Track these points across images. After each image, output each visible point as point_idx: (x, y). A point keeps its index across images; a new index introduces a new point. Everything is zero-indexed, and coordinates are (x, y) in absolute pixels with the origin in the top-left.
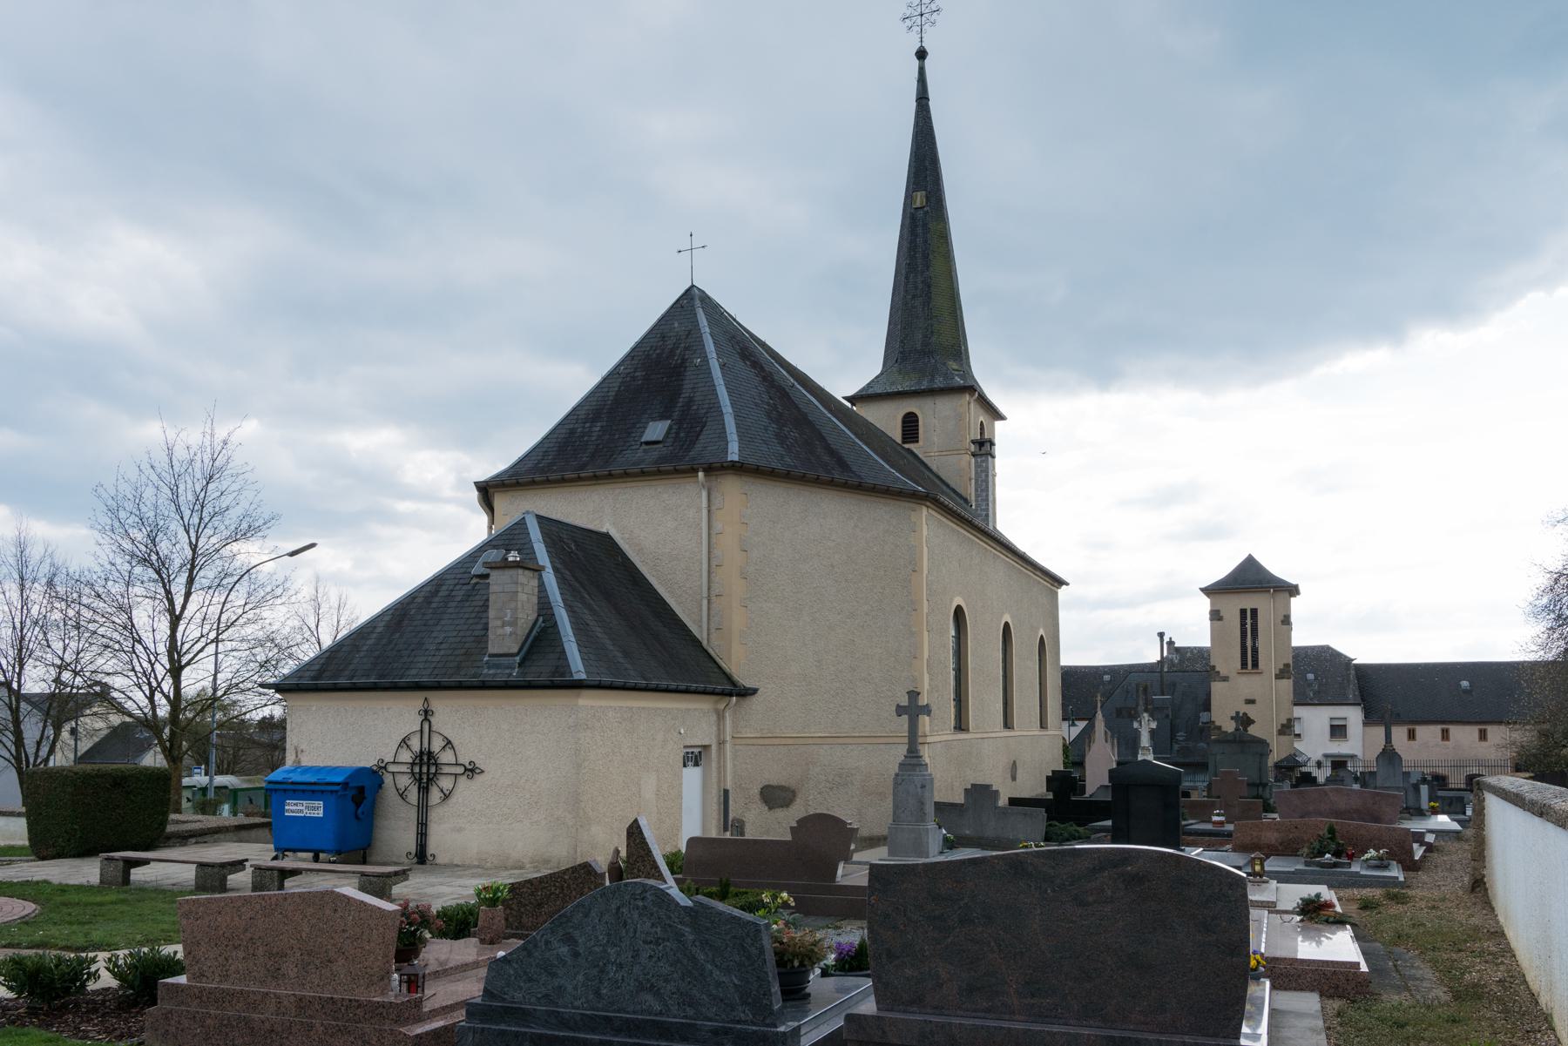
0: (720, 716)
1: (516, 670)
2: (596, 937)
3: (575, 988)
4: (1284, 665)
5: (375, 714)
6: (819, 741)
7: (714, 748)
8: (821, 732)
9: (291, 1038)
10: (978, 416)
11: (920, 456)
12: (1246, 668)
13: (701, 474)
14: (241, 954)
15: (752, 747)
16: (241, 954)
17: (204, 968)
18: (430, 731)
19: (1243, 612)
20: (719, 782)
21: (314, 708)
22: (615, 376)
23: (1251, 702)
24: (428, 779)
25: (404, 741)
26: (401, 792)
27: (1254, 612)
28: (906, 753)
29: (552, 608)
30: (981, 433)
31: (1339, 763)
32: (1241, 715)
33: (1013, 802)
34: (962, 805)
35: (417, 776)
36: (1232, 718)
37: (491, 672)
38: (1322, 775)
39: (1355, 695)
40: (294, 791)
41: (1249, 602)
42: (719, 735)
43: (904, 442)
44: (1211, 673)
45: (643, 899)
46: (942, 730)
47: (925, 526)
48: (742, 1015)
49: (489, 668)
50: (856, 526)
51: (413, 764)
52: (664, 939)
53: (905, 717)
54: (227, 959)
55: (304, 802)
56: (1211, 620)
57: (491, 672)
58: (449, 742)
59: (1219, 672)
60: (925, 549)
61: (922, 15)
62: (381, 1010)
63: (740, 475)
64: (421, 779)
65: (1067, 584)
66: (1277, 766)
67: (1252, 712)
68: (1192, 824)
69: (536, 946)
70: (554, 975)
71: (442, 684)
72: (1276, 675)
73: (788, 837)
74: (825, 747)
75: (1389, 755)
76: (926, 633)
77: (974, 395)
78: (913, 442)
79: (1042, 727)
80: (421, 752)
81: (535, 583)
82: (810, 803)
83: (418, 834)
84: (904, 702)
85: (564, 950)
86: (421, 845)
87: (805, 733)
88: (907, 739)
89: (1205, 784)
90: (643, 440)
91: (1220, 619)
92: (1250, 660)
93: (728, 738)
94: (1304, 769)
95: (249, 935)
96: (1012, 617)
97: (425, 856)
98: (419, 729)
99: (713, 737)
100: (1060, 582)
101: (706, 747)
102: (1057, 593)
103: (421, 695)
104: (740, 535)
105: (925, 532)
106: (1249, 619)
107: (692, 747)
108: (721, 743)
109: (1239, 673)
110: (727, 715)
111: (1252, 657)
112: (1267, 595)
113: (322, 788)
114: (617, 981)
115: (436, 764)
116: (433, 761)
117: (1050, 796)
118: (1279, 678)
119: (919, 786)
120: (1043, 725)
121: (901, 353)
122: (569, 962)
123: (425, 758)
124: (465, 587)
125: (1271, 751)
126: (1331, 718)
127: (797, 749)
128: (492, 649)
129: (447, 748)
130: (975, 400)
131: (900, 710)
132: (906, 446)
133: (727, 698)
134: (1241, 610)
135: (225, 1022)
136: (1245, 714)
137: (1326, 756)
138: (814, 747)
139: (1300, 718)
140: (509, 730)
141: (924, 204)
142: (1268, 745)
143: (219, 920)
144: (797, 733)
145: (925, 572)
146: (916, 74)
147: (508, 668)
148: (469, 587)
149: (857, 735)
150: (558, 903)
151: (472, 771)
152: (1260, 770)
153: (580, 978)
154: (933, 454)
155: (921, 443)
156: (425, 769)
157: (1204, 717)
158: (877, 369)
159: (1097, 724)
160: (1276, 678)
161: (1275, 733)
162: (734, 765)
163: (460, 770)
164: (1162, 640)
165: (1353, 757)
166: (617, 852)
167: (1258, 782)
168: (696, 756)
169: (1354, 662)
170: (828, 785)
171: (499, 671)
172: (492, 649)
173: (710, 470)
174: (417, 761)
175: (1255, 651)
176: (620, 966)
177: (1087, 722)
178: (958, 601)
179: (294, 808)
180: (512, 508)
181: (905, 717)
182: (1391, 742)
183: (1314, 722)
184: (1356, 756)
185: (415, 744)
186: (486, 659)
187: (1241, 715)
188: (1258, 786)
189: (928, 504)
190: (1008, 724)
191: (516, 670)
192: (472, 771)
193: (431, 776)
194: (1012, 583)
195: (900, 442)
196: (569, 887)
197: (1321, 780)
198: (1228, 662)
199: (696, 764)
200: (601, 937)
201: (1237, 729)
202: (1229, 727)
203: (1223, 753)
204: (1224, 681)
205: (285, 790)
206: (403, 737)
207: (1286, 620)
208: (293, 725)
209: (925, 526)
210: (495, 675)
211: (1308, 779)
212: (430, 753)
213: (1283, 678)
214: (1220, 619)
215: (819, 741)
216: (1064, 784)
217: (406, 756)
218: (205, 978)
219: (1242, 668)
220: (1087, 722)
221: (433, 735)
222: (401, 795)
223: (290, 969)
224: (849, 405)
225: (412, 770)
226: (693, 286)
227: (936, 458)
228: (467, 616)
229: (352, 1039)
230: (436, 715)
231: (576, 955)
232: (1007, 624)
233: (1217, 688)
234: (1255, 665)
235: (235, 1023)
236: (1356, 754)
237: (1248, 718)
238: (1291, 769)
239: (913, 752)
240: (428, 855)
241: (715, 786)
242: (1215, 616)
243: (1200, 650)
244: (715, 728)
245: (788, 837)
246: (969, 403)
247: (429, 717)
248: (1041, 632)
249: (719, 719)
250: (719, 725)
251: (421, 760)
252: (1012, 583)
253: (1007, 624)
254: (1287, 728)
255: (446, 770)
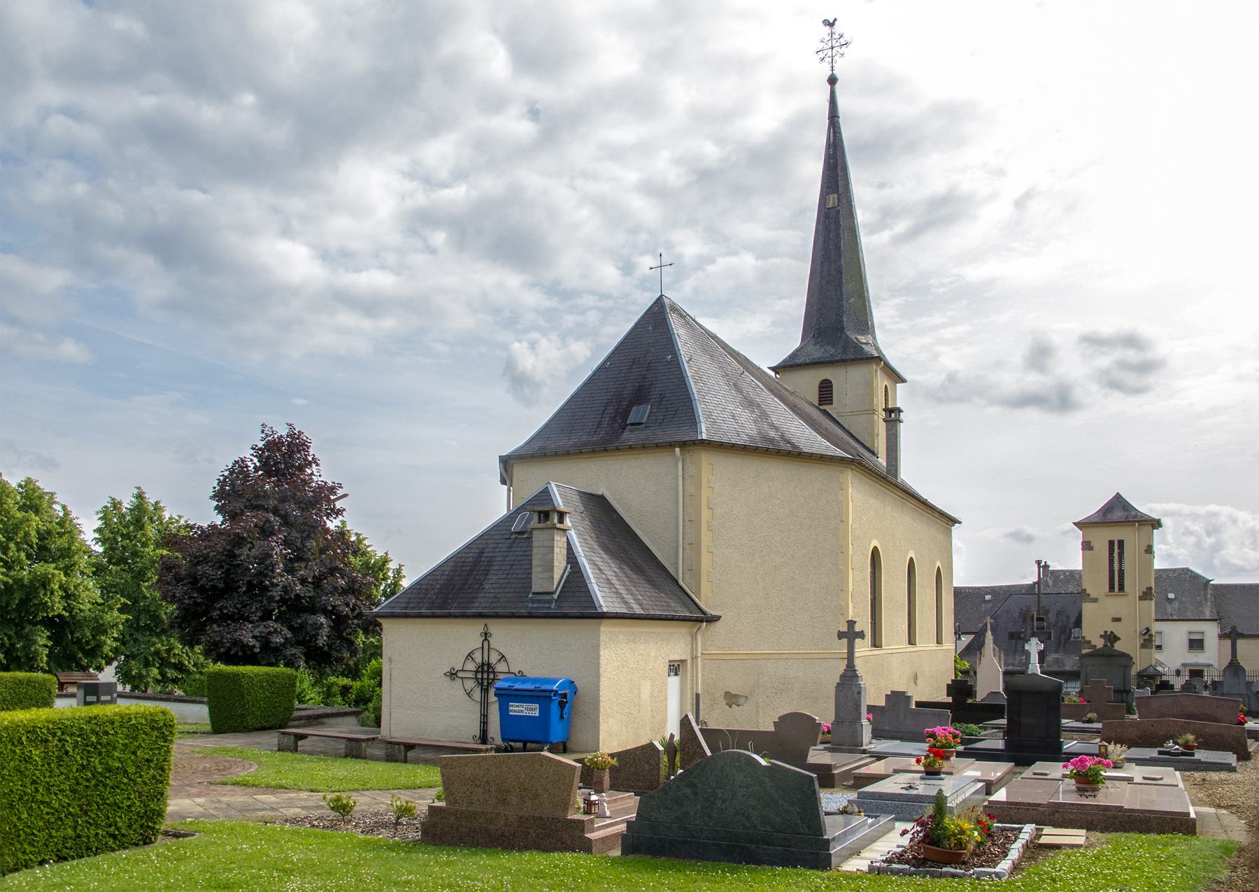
0: (694, 638)
1: (554, 604)
2: (709, 783)
3: (696, 814)
4: (1147, 588)
5: (447, 634)
6: (767, 657)
7: (689, 662)
8: (769, 650)
9: (515, 840)
10: (881, 381)
11: (834, 416)
12: (1114, 591)
13: (677, 450)
14: (480, 790)
15: (715, 661)
16: (480, 790)
17: (458, 798)
18: (489, 648)
19: (1111, 543)
20: (692, 688)
21: (403, 630)
22: (603, 370)
23: (1118, 620)
24: (488, 683)
25: (469, 655)
26: (468, 692)
27: (1121, 543)
28: (845, 668)
29: (576, 558)
30: (885, 404)
31: (1196, 673)
32: (1109, 633)
33: (919, 704)
34: (883, 707)
35: (480, 681)
36: (1101, 636)
37: (535, 605)
38: (1178, 683)
39: (1211, 611)
40: (517, 696)
41: (1116, 534)
42: (693, 651)
43: (820, 405)
44: (1083, 595)
45: (738, 762)
46: (862, 648)
47: (850, 485)
48: (802, 829)
49: (533, 603)
50: (797, 487)
51: (477, 672)
52: (752, 785)
53: (845, 641)
54: (471, 793)
55: (524, 704)
56: (1083, 549)
57: (535, 605)
58: (503, 657)
59: (1089, 595)
60: (851, 503)
61: (832, 48)
62: (573, 824)
63: (708, 450)
64: (482, 683)
65: (960, 523)
66: (1140, 675)
67: (1117, 629)
68: (1067, 723)
69: (670, 788)
70: (682, 805)
71: (500, 614)
72: (1139, 597)
73: (772, 729)
74: (772, 661)
75: (1234, 667)
76: (851, 571)
77: (880, 363)
78: (828, 404)
79: (938, 643)
80: (483, 664)
81: (565, 539)
82: (760, 705)
83: (481, 722)
84: (844, 628)
85: (688, 791)
86: (484, 731)
87: (756, 650)
88: (846, 654)
89: (1078, 690)
90: (628, 422)
91: (1091, 548)
92: (1117, 583)
93: (699, 655)
94: (1164, 678)
95: (485, 779)
96: (916, 554)
97: (487, 738)
98: (481, 646)
99: (688, 653)
100: (953, 521)
101: (683, 661)
102: (951, 530)
103: (482, 622)
104: (708, 497)
105: (850, 491)
106: (1116, 549)
107: (674, 661)
108: (694, 658)
109: (1106, 595)
110: (699, 637)
111: (1119, 582)
112: (1131, 528)
113: (540, 694)
114: (722, 809)
115: (494, 672)
116: (491, 670)
117: (950, 700)
118: (1142, 600)
119: (856, 693)
120: (939, 641)
121: (817, 329)
122: (692, 797)
123: (486, 668)
124: (507, 541)
125: (1134, 663)
126: (1189, 633)
127: (750, 663)
128: (535, 588)
129: (502, 661)
130: (881, 368)
131: (841, 635)
132: (822, 407)
133: (699, 623)
134: (1109, 541)
135: (473, 830)
136: (1112, 632)
137: (1184, 665)
138: (764, 661)
139: (1161, 633)
140: (548, 649)
141: (836, 205)
142: (1131, 658)
143: (466, 769)
144: (750, 650)
145: (850, 522)
146: (828, 97)
147: (547, 603)
148: (511, 541)
149: (797, 652)
150: (632, 769)
151: (453, 675)
152: (1124, 680)
153: (699, 807)
154: (844, 414)
155: (835, 404)
156: (485, 676)
157: (1075, 632)
158: (796, 343)
159: (986, 641)
160: (1139, 600)
161: (1138, 646)
162: (703, 675)
163: (460, 674)
164: (1039, 567)
165: (1209, 666)
166: (672, 736)
167: (1123, 689)
168: (676, 668)
169: (1211, 583)
170: (773, 691)
171: (540, 605)
172: (535, 588)
173: (683, 445)
174: (480, 670)
175: (1121, 572)
176: (724, 801)
177: (973, 636)
178: (875, 543)
179: (517, 709)
180: (532, 480)
181: (845, 641)
182: (1236, 657)
183: (1175, 635)
184: (1212, 665)
185: (478, 657)
186: (530, 596)
187: (1109, 633)
188: (1123, 692)
189: (853, 467)
190: (911, 641)
191: (554, 604)
192: (453, 675)
193: (490, 681)
194: (915, 525)
195: (817, 405)
196: (639, 759)
197: (1177, 687)
198: (1096, 585)
199: (676, 674)
200: (712, 784)
201: (1105, 646)
202: (1100, 643)
203: (1093, 665)
204: (1094, 602)
205: (509, 695)
206: (469, 652)
207: (1149, 550)
208: (388, 641)
209: (850, 485)
210: (537, 608)
211: (1166, 686)
212: (489, 664)
213: (1146, 599)
214: (1091, 548)
215: (767, 657)
216: (961, 689)
217: (471, 666)
218: (458, 804)
219: (1110, 591)
220: (973, 636)
221: (491, 651)
222: (468, 694)
223: (513, 800)
224: (772, 374)
225: (476, 676)
226: (662, 296)
227: (847, 417)
228: (511, 562)
229: (554, 841)
230: (493, 636)
231: (696, 794)
232: (911, 559)
233: (1087, 608)
234: (1121, 588)
235: (478, 831)
236: (1212, 663)
237: (1115, 636)
238: (1152, 677)
239: (851, 666)
240: (489, 738)
241: (689, 692)
242: (1087, 546)
243: (1072, 573)
244: (690, 647)
245: (772, 729)
246: (876, 371)
247: (488, 638)
248: (938, 564)
249: (692, 639)
250: (692, 644)
251: (483, 669)
252: (915, 525)
253: (911, 559)
254: (1148, 640)
255: (470, 675)
